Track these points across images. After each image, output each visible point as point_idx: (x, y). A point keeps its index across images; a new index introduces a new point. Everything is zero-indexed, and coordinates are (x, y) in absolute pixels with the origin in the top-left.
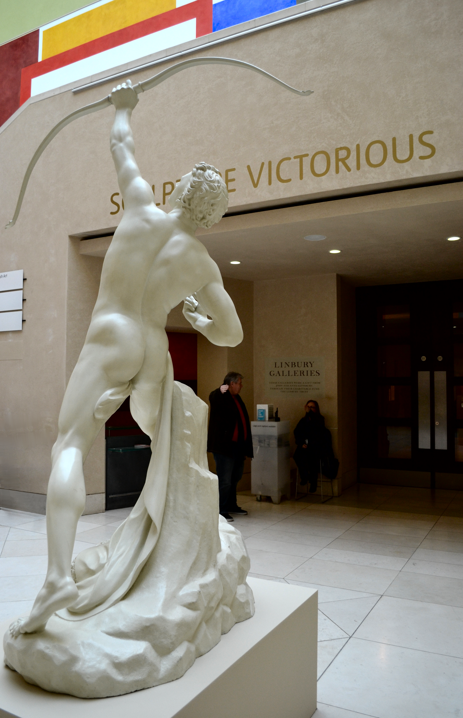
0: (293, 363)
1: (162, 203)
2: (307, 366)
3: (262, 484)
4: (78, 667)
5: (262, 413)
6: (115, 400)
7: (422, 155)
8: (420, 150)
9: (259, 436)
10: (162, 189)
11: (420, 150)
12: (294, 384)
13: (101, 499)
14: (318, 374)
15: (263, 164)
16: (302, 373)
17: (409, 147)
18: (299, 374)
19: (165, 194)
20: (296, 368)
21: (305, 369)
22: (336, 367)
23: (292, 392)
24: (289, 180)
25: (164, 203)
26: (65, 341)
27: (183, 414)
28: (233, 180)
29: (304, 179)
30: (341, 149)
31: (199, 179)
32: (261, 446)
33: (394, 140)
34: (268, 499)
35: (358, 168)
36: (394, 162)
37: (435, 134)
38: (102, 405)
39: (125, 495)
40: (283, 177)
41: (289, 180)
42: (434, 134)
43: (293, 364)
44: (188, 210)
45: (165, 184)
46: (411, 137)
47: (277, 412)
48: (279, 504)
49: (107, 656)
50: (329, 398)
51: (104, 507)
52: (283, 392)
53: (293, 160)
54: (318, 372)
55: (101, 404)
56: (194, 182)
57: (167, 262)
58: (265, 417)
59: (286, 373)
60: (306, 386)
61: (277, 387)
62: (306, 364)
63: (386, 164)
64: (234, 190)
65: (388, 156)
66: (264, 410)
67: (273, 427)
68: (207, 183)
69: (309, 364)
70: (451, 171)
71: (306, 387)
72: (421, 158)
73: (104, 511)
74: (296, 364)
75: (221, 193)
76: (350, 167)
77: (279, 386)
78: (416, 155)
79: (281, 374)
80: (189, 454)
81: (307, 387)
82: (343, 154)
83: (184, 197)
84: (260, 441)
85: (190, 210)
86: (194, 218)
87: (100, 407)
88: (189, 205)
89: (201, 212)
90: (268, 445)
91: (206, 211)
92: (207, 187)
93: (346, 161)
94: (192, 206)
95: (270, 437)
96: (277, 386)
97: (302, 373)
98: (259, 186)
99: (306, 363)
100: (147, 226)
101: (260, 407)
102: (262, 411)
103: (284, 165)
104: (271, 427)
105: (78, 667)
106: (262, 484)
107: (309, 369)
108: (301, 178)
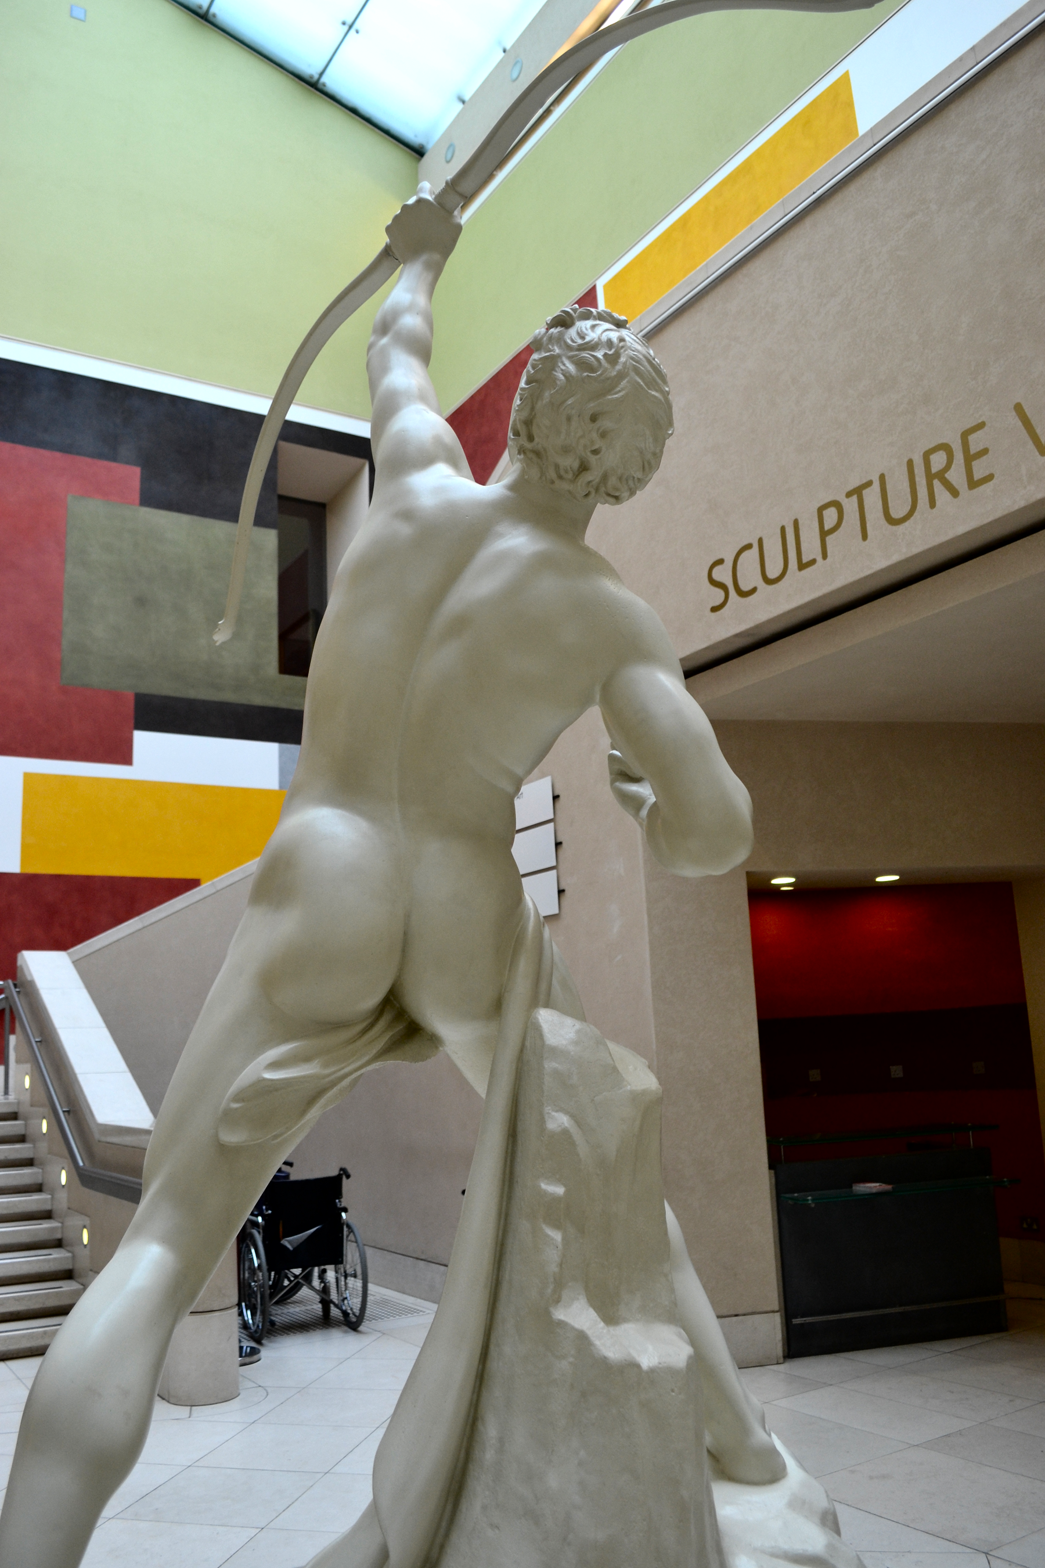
1: (819, 559)
6: (286, 1083)
13: (770, 1329)
19: (824, 534)
25: (825, 556)
26: (646, 929)
27: (542, 1121)
28: (985, 451)
29: (713, 614)
38: (243, 1100)
42: (1018, 398)
44: (531, 455)
45: (821, 510)
51: (779, 1349)
55: (236, 1098)
57: (460, 624)
64: (990, 478)
68: (570, 358)
73: (781, 1360)
75: (621, 376)
80: (553, 1268)
85: (537, 453)
86: (552, 474)
87: (235, 1105)
88: (531, 438)
89: (566, 450)
92: (571, 367)
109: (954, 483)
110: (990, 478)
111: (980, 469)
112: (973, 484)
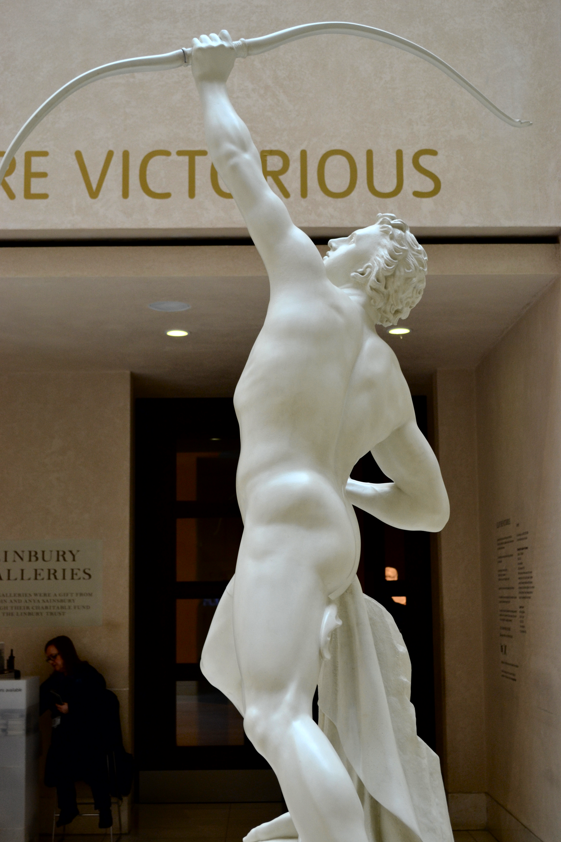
0: (33, 554)
2: (64, 560)
7: (419, 189)
8: (415, 181)
11: (415, 181)
15: (110, 154)
16: (52, 574)
17: (395, 172)
18: (46, 577)
20: (40, 564)
21: (59, 566)
23: (30, 614)
24: (167, 196)
28: (44, 175)
29: (197, 197)
30: (272, 153)
33: (370, 154)
35: (304, 193)
40: (152, 187)
41: (167, 196)
42: (439, 156)
43: (33, 556)
46: (399, 154)
47: (12, 658)
50: (111, 626)
52: (8, 614)
53: (174, 157)
54: (87, 571)
56: (396, 249)
59: (16, 573)
60: (62, 601)
62: (61, 556)
63: (354, 194)
64: (45, 196)
65: (358, 182)
68: (413, 254)
69: (68, 556)
71: (60, 604)
72: (417, 194)
74: (40, 555)
76: (289, 190)
78: (408, 187)
81: (63, 604)
82: (275, 163)
83: (378, 273)
91: (409, 300)
93: (282, 177)
94: (391, 289)
97: (52, 574)
98: (100, 196)
99: (61, 553)
100: (340, 319)
103: (155, 164)
104: (11, 690)
107: (69, 565)
108: (192, 194)
109: (12, 188)
110: (45, 196)
111: (37, 186)
112: (28, 195)
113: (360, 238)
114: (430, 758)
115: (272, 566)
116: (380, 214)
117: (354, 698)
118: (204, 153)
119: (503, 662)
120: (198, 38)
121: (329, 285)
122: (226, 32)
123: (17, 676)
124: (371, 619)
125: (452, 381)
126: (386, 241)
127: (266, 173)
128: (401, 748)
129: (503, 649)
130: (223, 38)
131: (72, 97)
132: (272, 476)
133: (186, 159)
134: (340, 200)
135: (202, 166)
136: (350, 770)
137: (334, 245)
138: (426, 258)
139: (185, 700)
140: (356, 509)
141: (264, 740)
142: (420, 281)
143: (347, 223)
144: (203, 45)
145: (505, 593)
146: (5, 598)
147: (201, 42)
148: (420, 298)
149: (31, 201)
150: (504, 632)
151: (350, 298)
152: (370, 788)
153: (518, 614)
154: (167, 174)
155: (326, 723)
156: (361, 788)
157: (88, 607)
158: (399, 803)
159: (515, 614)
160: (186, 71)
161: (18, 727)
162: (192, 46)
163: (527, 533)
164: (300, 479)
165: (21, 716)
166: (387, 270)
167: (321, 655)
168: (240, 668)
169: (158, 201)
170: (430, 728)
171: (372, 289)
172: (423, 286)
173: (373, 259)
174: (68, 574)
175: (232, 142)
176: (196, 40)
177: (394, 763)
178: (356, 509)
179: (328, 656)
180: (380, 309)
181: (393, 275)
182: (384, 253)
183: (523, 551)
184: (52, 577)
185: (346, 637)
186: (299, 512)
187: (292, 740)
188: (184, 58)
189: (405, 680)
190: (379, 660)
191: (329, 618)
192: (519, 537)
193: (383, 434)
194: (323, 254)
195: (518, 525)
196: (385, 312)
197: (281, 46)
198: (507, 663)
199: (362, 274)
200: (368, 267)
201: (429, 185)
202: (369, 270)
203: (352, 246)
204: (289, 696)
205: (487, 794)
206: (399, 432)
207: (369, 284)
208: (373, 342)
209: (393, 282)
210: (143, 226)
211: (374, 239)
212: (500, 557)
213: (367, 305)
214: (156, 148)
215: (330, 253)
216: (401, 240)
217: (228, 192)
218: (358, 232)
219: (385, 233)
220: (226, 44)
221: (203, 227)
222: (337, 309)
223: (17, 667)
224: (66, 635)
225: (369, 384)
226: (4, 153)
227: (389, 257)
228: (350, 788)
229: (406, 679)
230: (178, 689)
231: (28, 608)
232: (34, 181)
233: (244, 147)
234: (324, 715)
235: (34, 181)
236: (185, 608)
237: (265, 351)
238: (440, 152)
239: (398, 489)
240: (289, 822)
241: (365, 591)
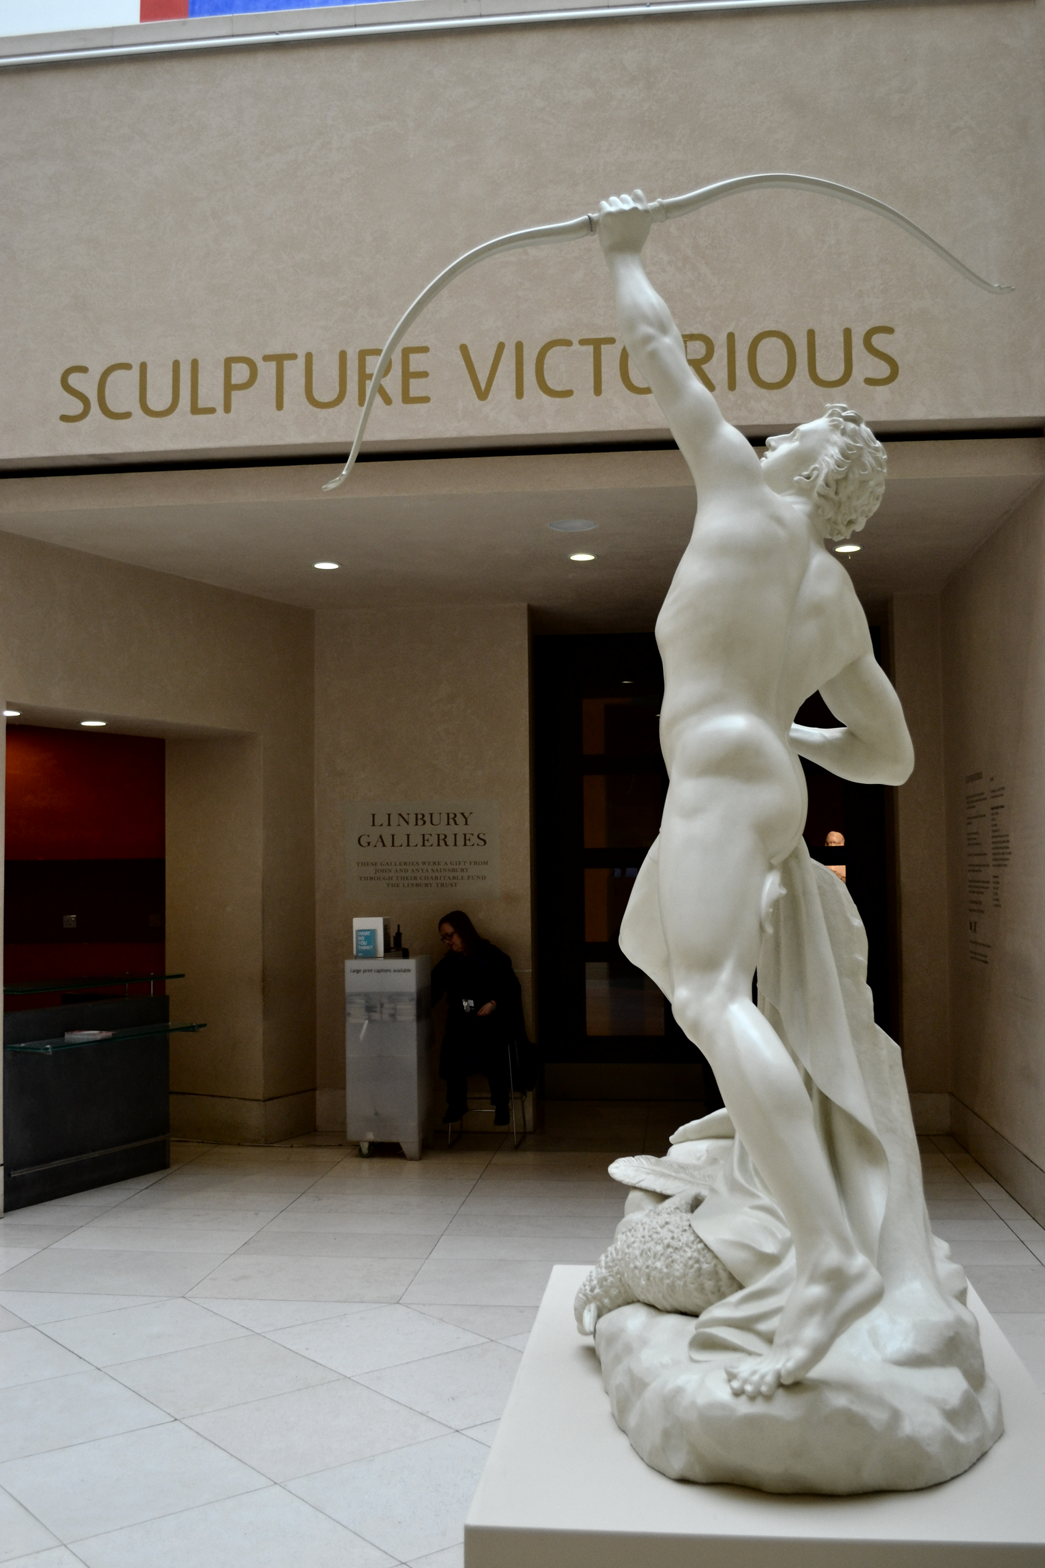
0: (420, 816)
3: (376, 1114)
4: (907, 1428)
5: (367, 938)
8: (866, 366)
9: (367, 996)
10: (221, 374)
11: (866, 366)
12: (421, 866)
14: (482, 843)
15: (501, 347)
17: (842, 355)
19: (229, 388)
20: (428, 828)
21: (450, 831)
22: (527, 825)
24: (569, 393)
25: (227, 409)
28: (424, 374)
31: (856, 442)
32: (371, 1021)
33: (811, 334)
34: (386, 1150)
35: (732, 385)
36: (812, 383)
37: (899, 334)
39: (46, 1167)
40: (551, 384)
41: (569, 393)
42: (896, 335)
43: (420, 819)
46: (847, 333)
48: (420, 1159)
49: (931, 1401)
53: (576, 346)
54: (481, 836)
56: (849, 447)
58: (375, 949)
59: (400, 839)
60: (454, 870)
61: (378, 874)
62: (451, 819)
63: (792, 384)
64: (425, 400)
65: (797, 370)
66: (373, 932)
67: (405, 971)
69: (460, 819)
70: (931, 418)
71: (451, 874)
72: (869, 381)
73: (2, 1215)
74: (427, 818)
76: (714, 382)
77: (382, 871)
79: (388, 841)
81: (455, 874)
84: (369, 1009)
90: (393, 1016)
93: (705, 367)
94: (843, 496)
95: (394, 997)
96: (377, 871)
98: (490, 397)
100: (782, 533)
101: (360, 923)
102: (367, 933)
103: (553, 356)
104: (399, 971)
105: (907, 1428)
106: (376, 1114)
107: (460, 829)
108: (598, 390)
110: (425, 400)
111: (417, 388)
112: (407, 399)
113: (805, 435)
114: (889, 1049)
115: (703, 826)
116: (828, 405)
117: (800, 978)
118: (611, 341)
119: (972, 942)
120: (607, 201)
121: (768, 491)
122: (639, 192)
123: (405, 955)
124: (819, 888)
125: (917, 602)
126: (837, 437)
127: (690, 362)
128: (856, 1037)
129: (973, 926)
130: (637, 199)
131: (457, 281)
132: (701, 720)
133: (590, 349)
134: (775, 391)
135: (610, 356)
136: (796, 1059)
137: (773, 444)
138: (885, 457)
139: (597, 984)
140: (803, 760)
141: (696, 1026)
142: (878, 485)
143: (784, 420)
144: (613, 209)
145: (976, 860)
146: (389, 867)
147: (610, 204)
148: (878, 505)
149: (409, 406)
150: (974, 906)
151: (794, 507)
152: (819, 1082)
153: (992, 885)
154: (568, 367)
155: (767, 1007)
156: (808, 1081)
157: (484, 878)
158: (853, 1099)
159: (986, 885)
160: (593, 242)
161: (408, 1012)
162: (600, 210)
163: (1003, 788)
164: (737, 723)
165: (411, 1000)
166: (838, 472)
167: (762, 928)
168: (666, 941)
169: (558, 400)
170: (888, 1015)
171: (820, 495)
172: (881, 490)
173: (820, 459)
174: (460, 840)
175: (650, 323)
176: (604, 203)
177: (848, 1053)
178: (803, 760)
179: (770, 930)
180: (829, 520)
181: (846, 478)
182: (834, 451)
183: (998, 810)
184: (442, 843)
185: (790, 909)
186: (736, 763)
187: (731, 1027)
188: (590, 225)
189: (861, 958)
190: (830, 935)
191: (771, 886)
192: (994, 794)
193: (834, 669)
194: (761, 455)
195: (992, 779)
196: (835, 523)
197: (703, 208)
198: (976, 943)
199: (808, 478)
200: (815, 469)
201: (884, 370)
202: (815, 473)
203: (795, 444)
204: (725, 975)
205: (951, 1094)
206: (853, 667)
207: (816, 489)
208: (820, 559)
209: (846, 487)
210: (541, 431)
211: (821, 434)
212: (969, 818)
213: (814, 516)
214: (555, 337)
215: (768, 453)
216: (854, 435)
217: (646, 386)
218: (803, 428)
219: (835, 427)
220: (640, 207)
221: (612, 429)
222: (778, 520)
223: (405, 944)
224: (460, 909)
225: (817, 609)
226: (381, 351)
227: (840, 456)
228: (798, 1079)
229: (862, 957)
230: (587, 971)
231: (415, 878)
232: (413, 382)
233: (663, 329)
234: (764, 999)
235: (413, 382)
236: (596, 880)
237: (692, 572)
238: (897, 330)
239: (851, 735)
240: (726, 1119)
241: (812, 856)
